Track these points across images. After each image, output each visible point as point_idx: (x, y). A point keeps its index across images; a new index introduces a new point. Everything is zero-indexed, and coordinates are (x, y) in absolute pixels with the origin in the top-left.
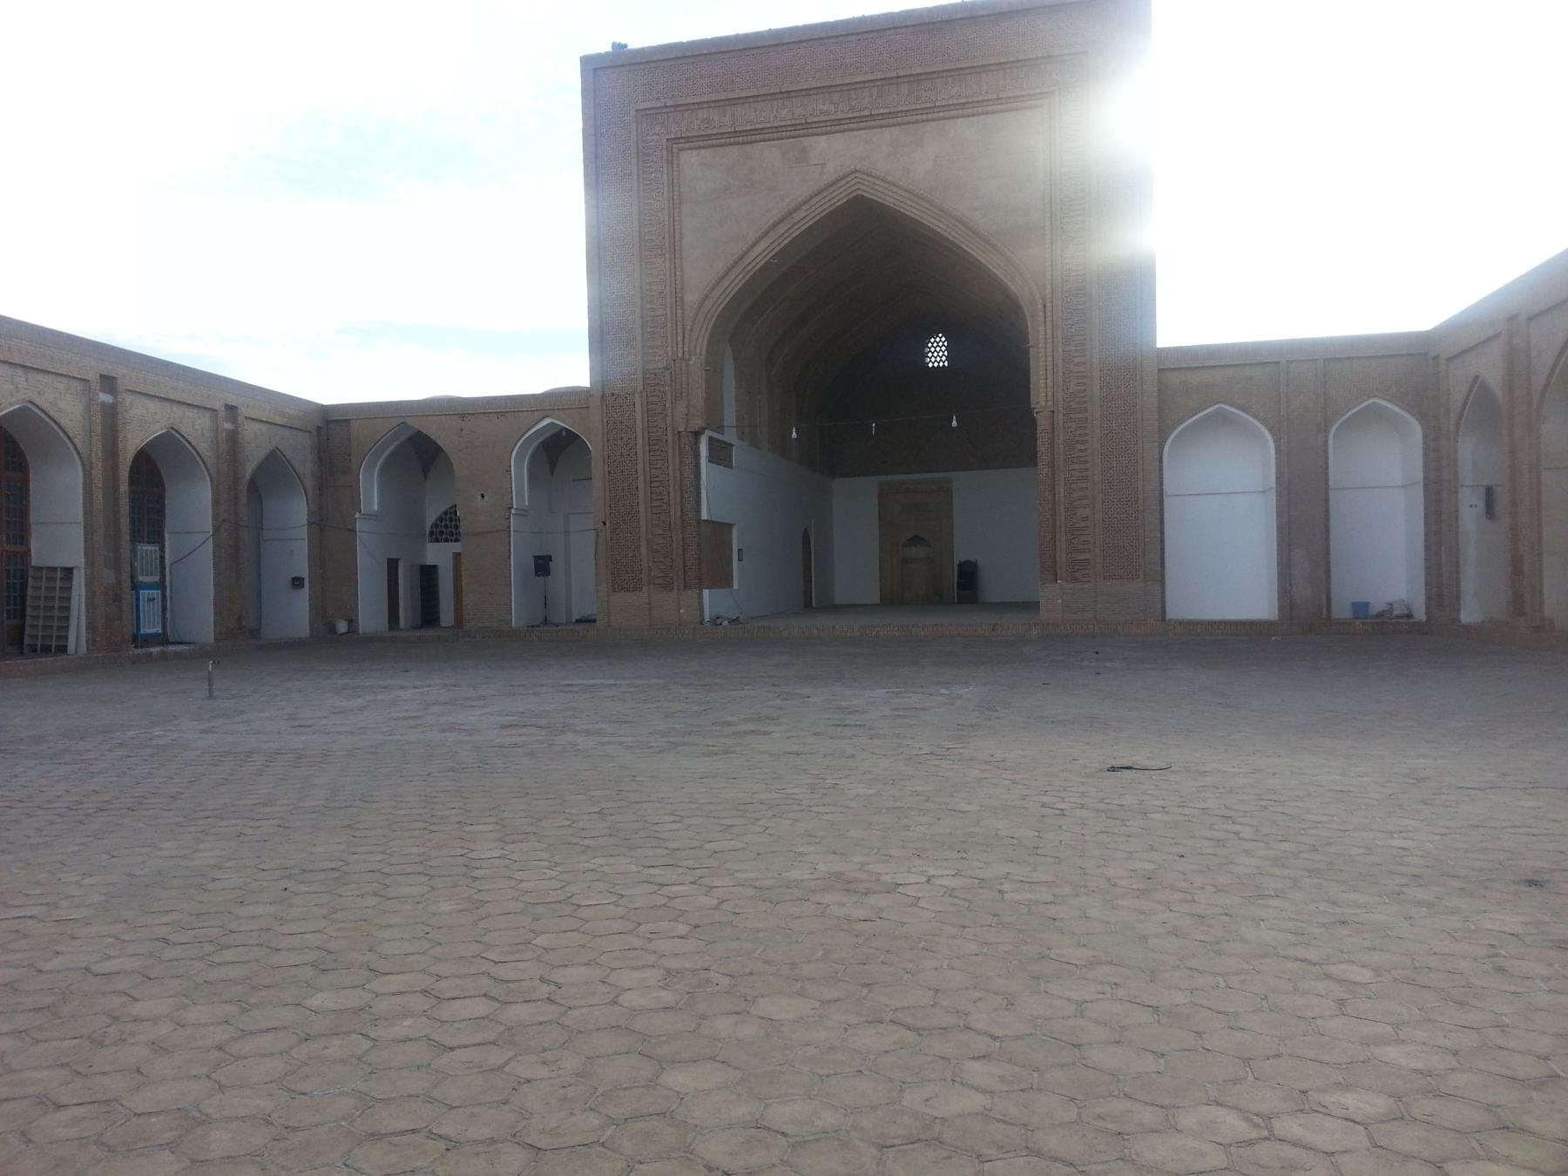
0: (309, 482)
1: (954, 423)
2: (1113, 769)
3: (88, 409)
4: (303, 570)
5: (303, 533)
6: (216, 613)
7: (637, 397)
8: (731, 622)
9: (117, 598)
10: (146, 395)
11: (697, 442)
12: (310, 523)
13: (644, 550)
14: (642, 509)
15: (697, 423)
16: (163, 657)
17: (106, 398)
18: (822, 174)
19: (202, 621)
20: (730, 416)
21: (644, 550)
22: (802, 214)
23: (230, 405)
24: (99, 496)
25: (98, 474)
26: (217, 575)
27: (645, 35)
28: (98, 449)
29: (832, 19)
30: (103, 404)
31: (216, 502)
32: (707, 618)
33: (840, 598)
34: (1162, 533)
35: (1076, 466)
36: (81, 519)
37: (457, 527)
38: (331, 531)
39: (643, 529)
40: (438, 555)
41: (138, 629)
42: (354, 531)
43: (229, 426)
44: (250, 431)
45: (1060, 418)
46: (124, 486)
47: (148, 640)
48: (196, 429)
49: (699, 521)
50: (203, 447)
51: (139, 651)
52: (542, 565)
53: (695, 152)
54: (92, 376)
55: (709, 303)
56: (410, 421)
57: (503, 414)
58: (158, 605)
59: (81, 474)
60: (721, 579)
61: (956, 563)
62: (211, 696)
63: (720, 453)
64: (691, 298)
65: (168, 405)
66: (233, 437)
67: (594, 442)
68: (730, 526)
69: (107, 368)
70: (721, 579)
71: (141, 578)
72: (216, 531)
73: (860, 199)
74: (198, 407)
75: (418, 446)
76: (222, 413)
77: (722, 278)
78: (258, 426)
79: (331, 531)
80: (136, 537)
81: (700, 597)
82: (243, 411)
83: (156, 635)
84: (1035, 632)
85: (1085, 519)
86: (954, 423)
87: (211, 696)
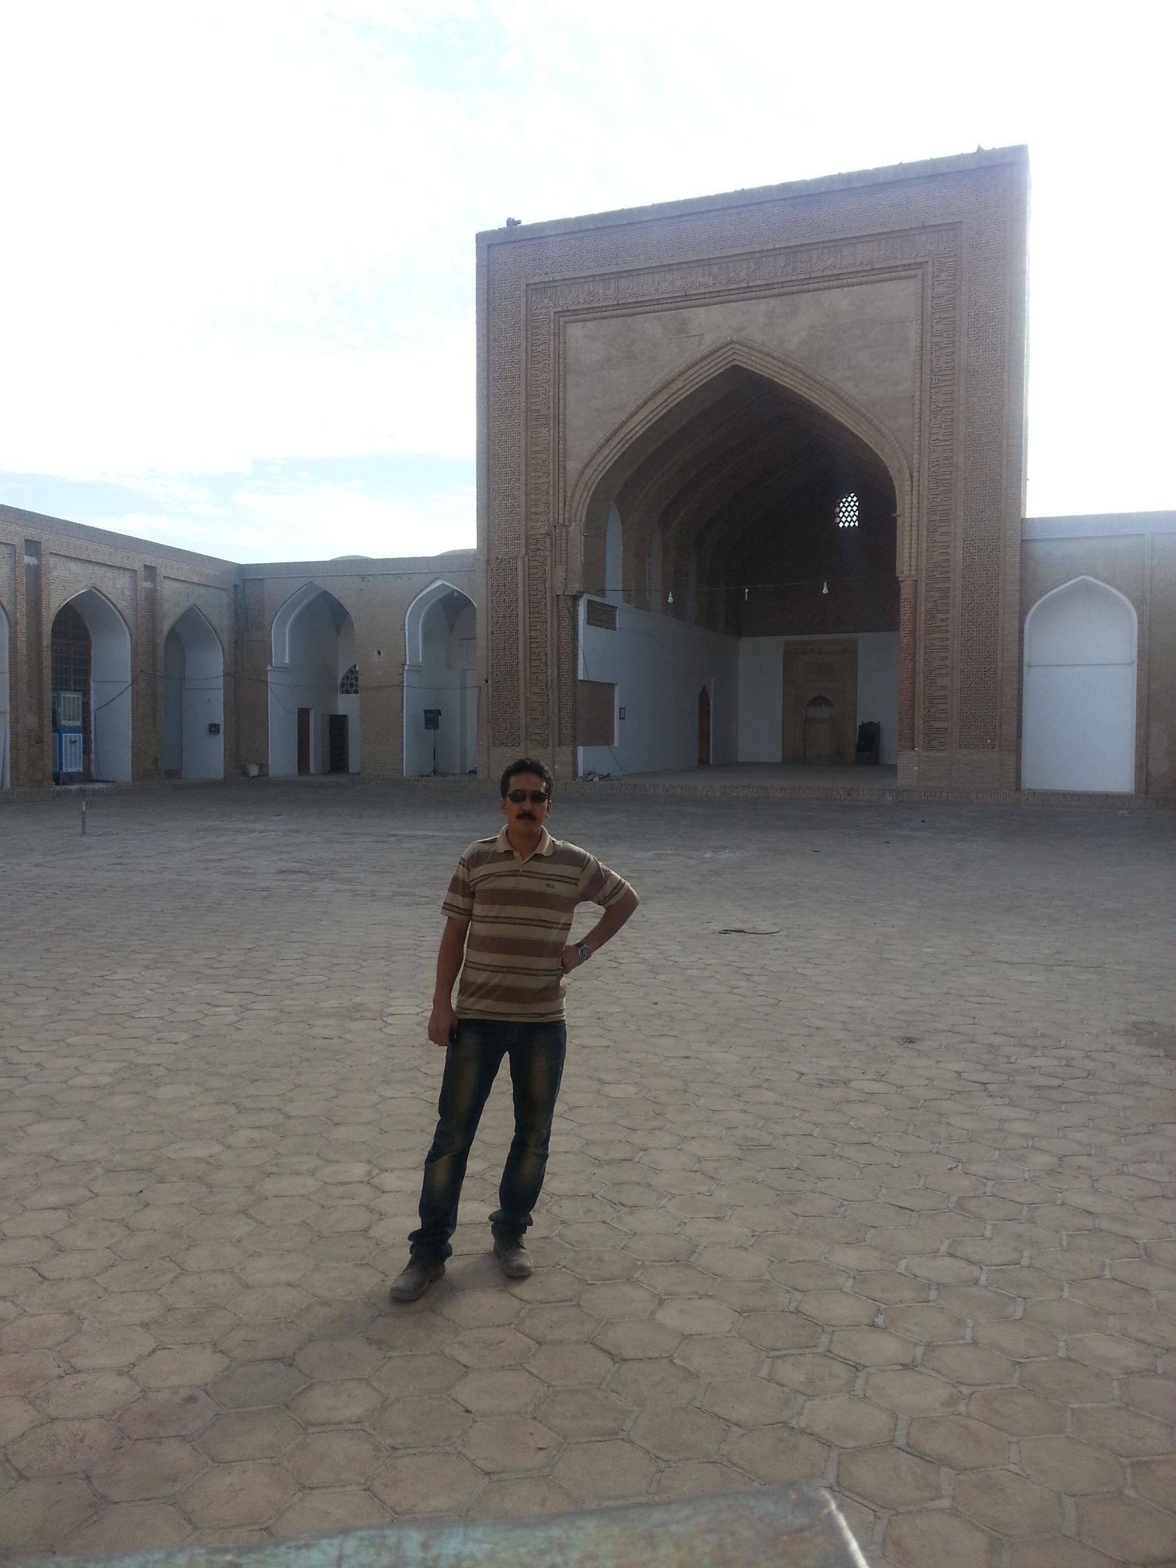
0: (226, 637)
1: (825, 591)
2: (726, 932)
3: (13, 570)
4: (220, 720)
5: (220, 683)
6: (133, 756)
7: (520, 561)
8: (603, 778)
9: (40, 741)
10: (69, 557)
11: (575, 606)
12: (226, 674)
13: (522, 707)
14: (521, 667)
15: (576, 587)
16: (82, 794)
17: (29, 560)
18: (699, 345)
19: (120, 760)
20: (614, 577)
21: (522, 707)
22: (679, 384)
23: (150, 562)
24: (22, 646)
25: (22, 628)
26: (135, 720)
27: (539, 208)
28: (23, 607)
29: (712, 193)
30: (28, 566)
31: (135, 654)
32: (581, 774)
33: (741, 758)
34: (1020, 704)
35: (937, 635)
36: (7, 668)
37: (356, 679)
38: (245, 680)
39: (522, 690)
40: (346, 705)
41: (61, 768)
42: (266, 682)
43: (148, 585)
44: (167, 589)
45: (922, 588)
46: (47, 639)
47: (72, 778)
48: (117, 589)
49: (575, 680)
50: (123, 604)
51: (58, 788)
52: (432, 719)
53: (580, 325)
54: (18, 541)
55: (589, 471)
56: (317, 582)
57: (399, 576)
58: (80, 745)
59: (7, 628)
60: (602, 736)
61: (859, 723)
62: (84, 833)
63: (601, 616)
64: (573, 466)
65: (90, 567)
66: (152, 597)
67: (479, 602)
68: (611, 686)
69: (33, 534)
70: (602, 736)
71: (65, 723)
72: (135, 681)
73: (735, 372)
74: (119, 568)
75: (326, 604)
76: (142, 573)
77: (602, 447)
78: (176, 585)
79: (245, 680)
80: (60, 684)
81: (574, 754)
82: (162, 571)
83: (79, 773)
84: (889, 798)
85: (945, 688)
86: (825, 591)
87: (84, 833)
